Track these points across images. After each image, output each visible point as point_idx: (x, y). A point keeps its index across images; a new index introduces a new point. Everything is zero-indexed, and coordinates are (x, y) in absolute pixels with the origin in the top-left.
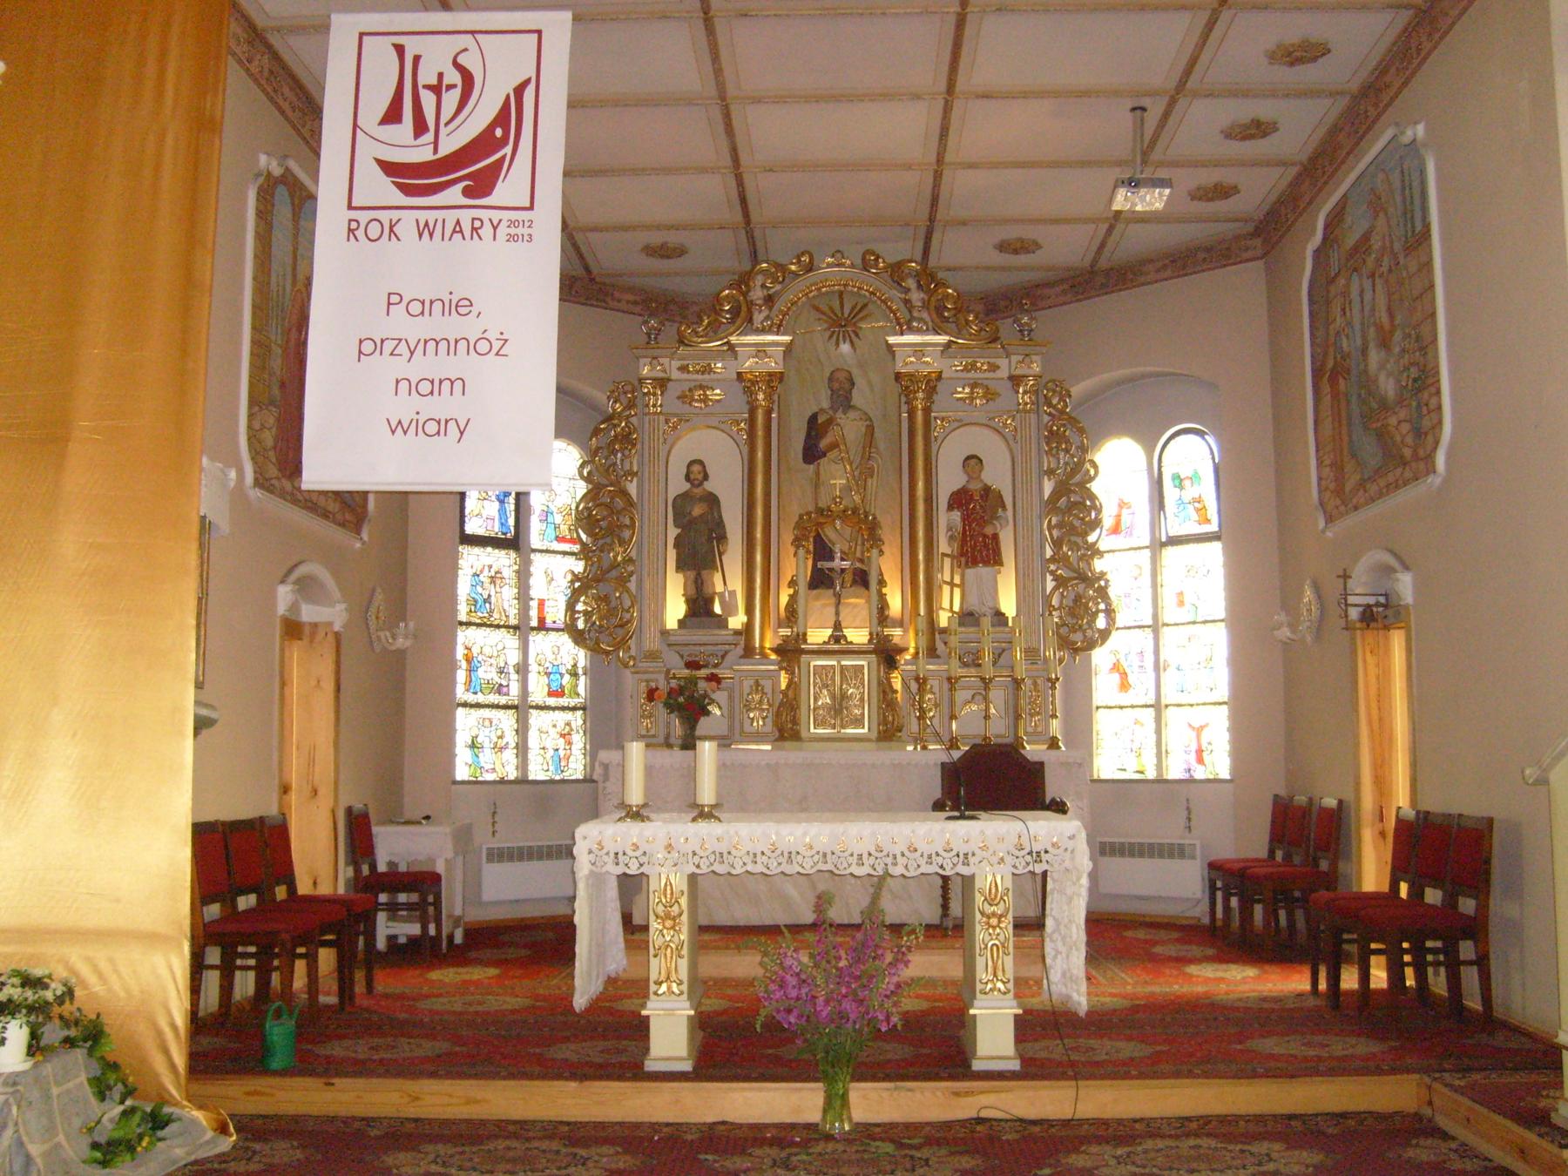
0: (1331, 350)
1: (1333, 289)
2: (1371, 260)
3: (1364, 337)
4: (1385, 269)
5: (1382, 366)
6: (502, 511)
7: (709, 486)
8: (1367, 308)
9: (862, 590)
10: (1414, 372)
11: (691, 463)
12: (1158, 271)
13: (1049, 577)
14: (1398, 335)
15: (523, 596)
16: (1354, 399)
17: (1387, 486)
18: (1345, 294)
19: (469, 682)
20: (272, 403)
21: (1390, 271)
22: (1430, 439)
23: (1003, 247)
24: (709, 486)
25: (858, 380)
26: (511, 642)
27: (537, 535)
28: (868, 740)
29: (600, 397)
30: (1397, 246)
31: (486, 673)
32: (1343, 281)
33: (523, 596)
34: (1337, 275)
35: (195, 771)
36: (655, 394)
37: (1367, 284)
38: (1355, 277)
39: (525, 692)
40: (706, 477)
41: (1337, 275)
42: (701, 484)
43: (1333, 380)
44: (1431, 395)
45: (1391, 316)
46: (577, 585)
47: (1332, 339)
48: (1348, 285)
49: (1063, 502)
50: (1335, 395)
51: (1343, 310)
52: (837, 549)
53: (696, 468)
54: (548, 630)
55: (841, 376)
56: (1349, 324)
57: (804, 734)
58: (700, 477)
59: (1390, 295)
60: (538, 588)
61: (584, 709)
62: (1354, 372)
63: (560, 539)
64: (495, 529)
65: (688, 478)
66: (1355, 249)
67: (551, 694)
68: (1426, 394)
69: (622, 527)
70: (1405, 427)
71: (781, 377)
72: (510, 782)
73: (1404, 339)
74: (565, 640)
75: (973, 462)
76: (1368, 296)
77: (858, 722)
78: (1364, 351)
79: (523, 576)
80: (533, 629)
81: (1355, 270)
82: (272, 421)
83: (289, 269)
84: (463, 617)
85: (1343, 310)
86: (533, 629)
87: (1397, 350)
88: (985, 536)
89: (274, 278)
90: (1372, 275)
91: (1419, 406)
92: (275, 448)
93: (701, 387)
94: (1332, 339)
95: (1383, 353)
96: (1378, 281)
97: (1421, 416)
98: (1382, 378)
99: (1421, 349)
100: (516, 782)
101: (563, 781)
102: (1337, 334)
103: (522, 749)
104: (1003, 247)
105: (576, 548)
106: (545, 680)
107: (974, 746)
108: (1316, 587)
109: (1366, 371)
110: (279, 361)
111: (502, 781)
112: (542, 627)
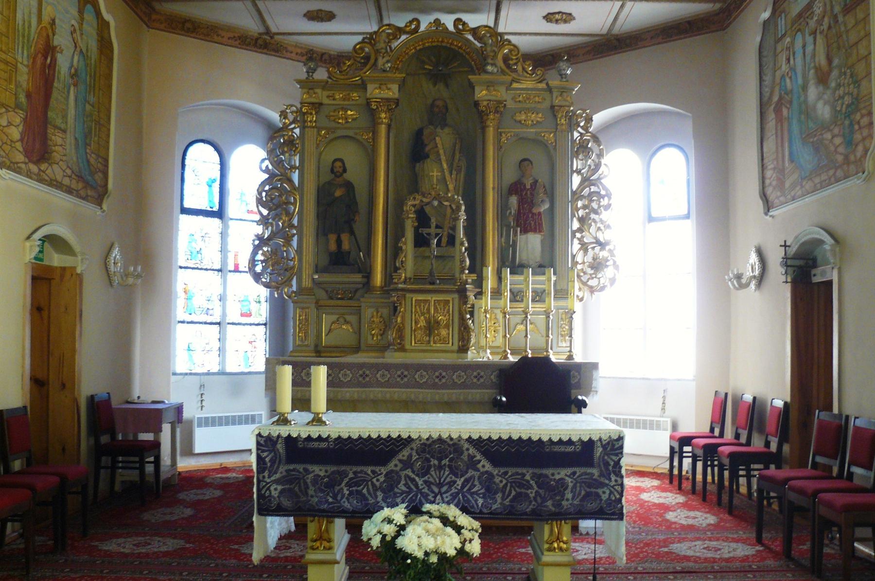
0: (777, 89)
1: (779, 47)
2: (812, 23)
3: (805, 77)
4: (825, 26)
5: (819, 98)
6: (210, 193)
7: (347, 176)
8: (808, 58)
9: (324, 261)
10: (847, 100)
11: (335, 160)
12: (652, 38)
13: (576, 241)
14: (835, 73)
15: (224, 250)
16: (795, 122)
17: (821, 183)
18: (790, 48)
19: (186, 306)
20: (18, 106)
21: (830, 28)
22: (860, 148)
23: (549, 18)
24: (347, 176)
25: (450, 106)
26: (216, 277)
27: (232, 210)
28: (452, 352)
29: (274, 116)
30: (837, 9)
31: (199, 301)
32: (788, 40)
33: (224, 250)
34: (784, 36)
35: (31, 356)
36: (311, 114)
37: (809, 39)
38: (799, 36)
39: (224, 315)
40: (345, 171)
41: (784, 36)
42: (341, 175)
43: (778, 111)
44: (862, 116)
45: (830, 60)
46: (257, 242)
47: (778, 80)
48: (792, 43)
49: (586, 192)
50: (325, 352)
51: (788, 60)
52: (433, 220)
53: (338, 164)
54: (241, 272)
55: (440, 103)
56: (793, 69)
57: (407, 347)
58: (341, 170)
59: (828, 46)
60: (232, 246)
61: (265, 324)
62: (795, 103)
63: (249, 212)
64: (204, 206)
65: (332, 171)
66: (800, 15)
67: (243, 315)
68: (858, 116)
69: (288, 203)
70: (838, 141)
71: (397, 102)
72: (214, 374)
73: (840, 76)
74: (248, 278)
75: (526, 163)
76: (810, 48)
77: (445, 341)
78: (805, 88)
79: (224, 235)
80: (230, 271)
81: (799, 30)
82: (18, 120)
83: (35, 10)
84: (182, 262)
85: (788, 60)
86: (230, 271)
87: (833, 85)
88: (533, 214)
89: (19, 16)
90: (814, 33)
91: (851, 125)
92: (22, 140)
93: (343, 109)
94: (778, 80)
95: (821, 88)
96: (818, 36)
97: (852, 132)
98: (820, 105)
99: (855, 82)
100: (218, 374)
101: (250, 373)
102: (783, 77)
103: (222, 351)
104: (549, 18)
105: (257, 217)
106: (239, 305)
107: (524, 360)
108: (760, 253)
109: (806, 101)
110: (26, 77)
111: (208, 374)
112: (236, 270)
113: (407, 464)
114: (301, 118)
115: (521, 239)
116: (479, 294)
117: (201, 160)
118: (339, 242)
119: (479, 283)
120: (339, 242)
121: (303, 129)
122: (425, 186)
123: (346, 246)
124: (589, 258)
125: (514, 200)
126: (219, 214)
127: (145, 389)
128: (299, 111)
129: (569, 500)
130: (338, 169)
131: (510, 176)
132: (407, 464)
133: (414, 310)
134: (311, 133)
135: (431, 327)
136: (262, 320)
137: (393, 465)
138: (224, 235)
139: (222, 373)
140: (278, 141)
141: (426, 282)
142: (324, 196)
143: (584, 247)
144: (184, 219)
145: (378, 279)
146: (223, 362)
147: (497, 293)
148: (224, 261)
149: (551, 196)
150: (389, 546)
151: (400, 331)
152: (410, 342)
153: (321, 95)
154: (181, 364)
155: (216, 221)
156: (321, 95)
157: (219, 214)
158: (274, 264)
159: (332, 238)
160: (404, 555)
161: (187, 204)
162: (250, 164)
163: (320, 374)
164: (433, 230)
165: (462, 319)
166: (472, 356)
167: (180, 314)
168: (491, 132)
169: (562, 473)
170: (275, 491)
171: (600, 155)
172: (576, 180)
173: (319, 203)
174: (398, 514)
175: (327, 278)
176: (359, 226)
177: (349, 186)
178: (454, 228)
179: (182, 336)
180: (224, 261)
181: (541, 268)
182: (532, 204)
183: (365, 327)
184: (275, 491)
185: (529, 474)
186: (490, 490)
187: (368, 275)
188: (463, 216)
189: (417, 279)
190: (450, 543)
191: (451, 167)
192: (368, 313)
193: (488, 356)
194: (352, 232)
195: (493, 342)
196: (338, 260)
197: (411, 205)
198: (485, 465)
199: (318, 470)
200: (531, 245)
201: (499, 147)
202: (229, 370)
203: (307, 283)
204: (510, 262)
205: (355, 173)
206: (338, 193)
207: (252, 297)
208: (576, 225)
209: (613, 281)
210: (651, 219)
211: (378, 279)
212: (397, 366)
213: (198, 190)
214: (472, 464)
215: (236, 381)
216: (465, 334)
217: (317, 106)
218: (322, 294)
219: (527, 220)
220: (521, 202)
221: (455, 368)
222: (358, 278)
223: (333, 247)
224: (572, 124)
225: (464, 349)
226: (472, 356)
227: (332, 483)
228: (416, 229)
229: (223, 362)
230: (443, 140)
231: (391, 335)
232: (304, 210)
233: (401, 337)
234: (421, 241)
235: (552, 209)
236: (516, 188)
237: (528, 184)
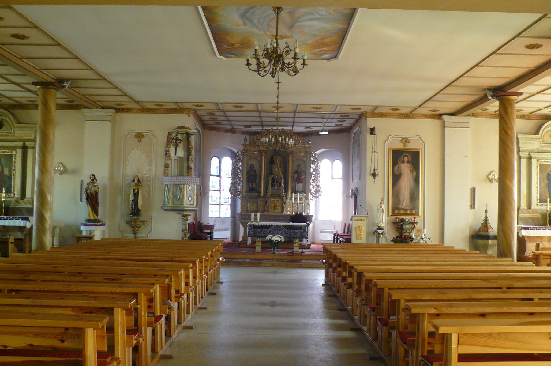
7: (254, 169)
15: (220, 185)
24: (254, 169)
26: (218, 192)
27: (222, 175)
29: (236, 151)
33: (220, 185)
79: (220, 181)
107: (296, 215)
113: (273, 229)
114: (243, 153)
115: (297, 185)
116: (287, 199)
117: (215, 161)
118: (252, 185)
119: (287, 196)
120: (252, 185)
121: (243, 156)
122: (273, 173)
123: (254, 186)
124: (314, 190)
125: (296, 175)
126: (219, 176)
127: (204, 221)
128: (242, 152)
129: (298, 235)
130: (252, 166)
131: (295, 168)
132: (273, 229)
133: (271, 202)
134: (245, 157)
135: (275, 207)
136: (229, 204)
137: (270, 229)
138: (220, 181)
139: (219, 218)
140: (234, 156)
141: (274, 195)
142: (248, 172)
143: (313, 187)
144: (211, 177)
145: (262, 194)
146: (220, 215)
147: (291, 198)
148: (220, 188)
149: (305, 174)
150: (270, 239)
151: (268, 207)
152: (270, 210)
153: (248, 148)
154: (210, 216)
155: (218, 178)
156: (248, 148)
157: (219, 176)
158: (233, 190)
159: (251, 184)
160: (272, 241)
161: (212, 173)
162: (227, 163)
163: (258, 215)
164: (276, 183)
165: (282, 205)
166: (284, 213)
167: (210, 202)
168: (290, 159)
169: (297, 231)
170: (251, 233)
171: (318, 164)
172: (312, 170)
173: (247, 174)
174: (272, 236)
175: (249, 194)
176: (257, 181)
177: (255, 171)
178: (281, 182)
179: (211, 208)
180: (220, 188)
181: (302, 192)
182: (300, 176)
183: (259, 206)
184: (251, 233)
185: (292, 231)
186: (286, 233)
187: (260, 193)
188: (283, 180)
189: (272, 195)
190: (279, 239)
191: (280, 166)
192: (259, 203)
193: (289, 213)
194: (255, 182)
195: (289, 211)
196: (252, 190)
197: (270, 177)
198: (285, 229)
199: (258, 230)
200: (300, 186)
201: (292, 161)
202: (221, 217)
203: (244, 195)
204: (295, 191)
205: (256, 168)
206: (252, 173)
207: (227, 196)
208: (311, 181)
209: (320, 195)
210: (333, 179)
211: (262, 194)
212: (267, 215)
213: (214, 170)
214: (283, 229)
215: (223, 220)
216: (283, 208)
217: (247, 151)
218: (248, 198)
219: (299, 180)
220: (298, 175)
221: (281, 216)
222: (257, 194)
223: (251, 186)
224: (311, 156)
225: (283, 212)
226: (284, 213)
227: (260, 232)
228: (272, 183)
229: (220, 215)
230: (278, 160)
231: (266, 208)
232: (242, 176)
233: (268, 209)
234: (272, 185)
235: (305, 177)
236: (296, 172)
237: (299, 171)
